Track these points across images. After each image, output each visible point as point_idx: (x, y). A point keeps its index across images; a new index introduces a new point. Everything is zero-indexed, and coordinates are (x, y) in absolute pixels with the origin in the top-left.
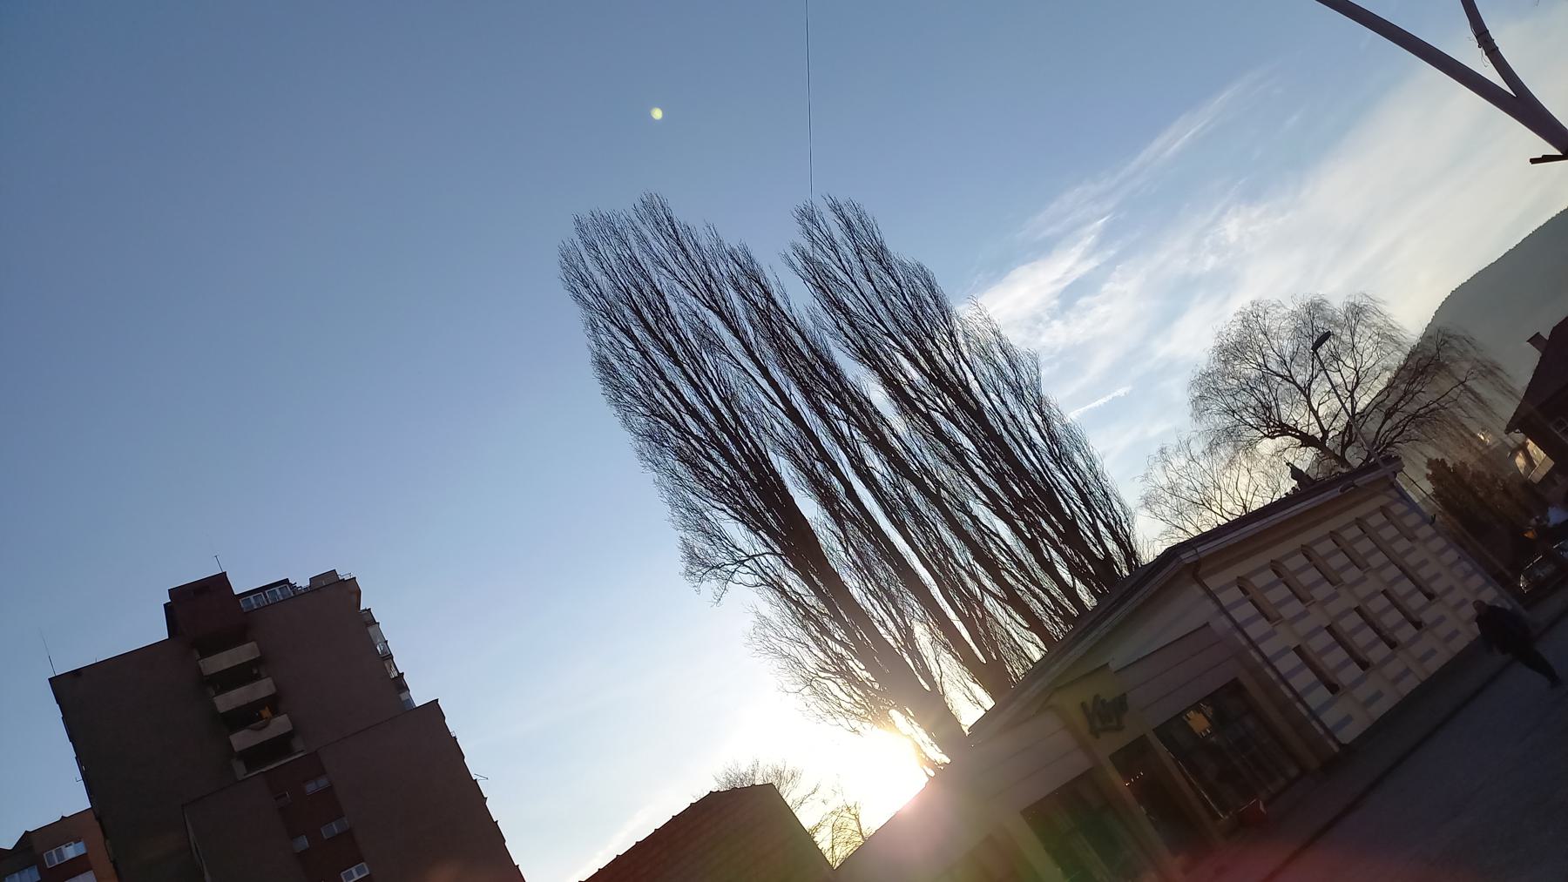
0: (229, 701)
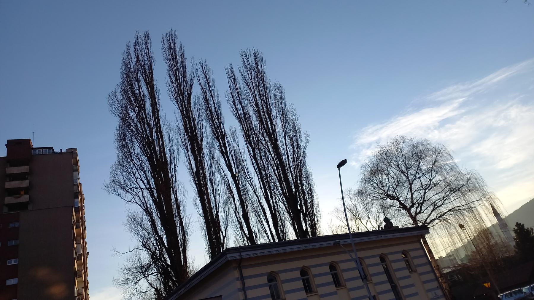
0: (9, 185)
